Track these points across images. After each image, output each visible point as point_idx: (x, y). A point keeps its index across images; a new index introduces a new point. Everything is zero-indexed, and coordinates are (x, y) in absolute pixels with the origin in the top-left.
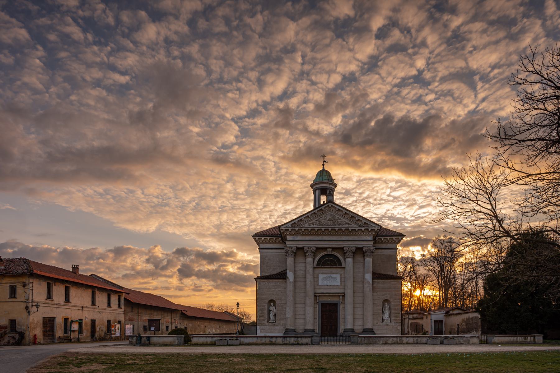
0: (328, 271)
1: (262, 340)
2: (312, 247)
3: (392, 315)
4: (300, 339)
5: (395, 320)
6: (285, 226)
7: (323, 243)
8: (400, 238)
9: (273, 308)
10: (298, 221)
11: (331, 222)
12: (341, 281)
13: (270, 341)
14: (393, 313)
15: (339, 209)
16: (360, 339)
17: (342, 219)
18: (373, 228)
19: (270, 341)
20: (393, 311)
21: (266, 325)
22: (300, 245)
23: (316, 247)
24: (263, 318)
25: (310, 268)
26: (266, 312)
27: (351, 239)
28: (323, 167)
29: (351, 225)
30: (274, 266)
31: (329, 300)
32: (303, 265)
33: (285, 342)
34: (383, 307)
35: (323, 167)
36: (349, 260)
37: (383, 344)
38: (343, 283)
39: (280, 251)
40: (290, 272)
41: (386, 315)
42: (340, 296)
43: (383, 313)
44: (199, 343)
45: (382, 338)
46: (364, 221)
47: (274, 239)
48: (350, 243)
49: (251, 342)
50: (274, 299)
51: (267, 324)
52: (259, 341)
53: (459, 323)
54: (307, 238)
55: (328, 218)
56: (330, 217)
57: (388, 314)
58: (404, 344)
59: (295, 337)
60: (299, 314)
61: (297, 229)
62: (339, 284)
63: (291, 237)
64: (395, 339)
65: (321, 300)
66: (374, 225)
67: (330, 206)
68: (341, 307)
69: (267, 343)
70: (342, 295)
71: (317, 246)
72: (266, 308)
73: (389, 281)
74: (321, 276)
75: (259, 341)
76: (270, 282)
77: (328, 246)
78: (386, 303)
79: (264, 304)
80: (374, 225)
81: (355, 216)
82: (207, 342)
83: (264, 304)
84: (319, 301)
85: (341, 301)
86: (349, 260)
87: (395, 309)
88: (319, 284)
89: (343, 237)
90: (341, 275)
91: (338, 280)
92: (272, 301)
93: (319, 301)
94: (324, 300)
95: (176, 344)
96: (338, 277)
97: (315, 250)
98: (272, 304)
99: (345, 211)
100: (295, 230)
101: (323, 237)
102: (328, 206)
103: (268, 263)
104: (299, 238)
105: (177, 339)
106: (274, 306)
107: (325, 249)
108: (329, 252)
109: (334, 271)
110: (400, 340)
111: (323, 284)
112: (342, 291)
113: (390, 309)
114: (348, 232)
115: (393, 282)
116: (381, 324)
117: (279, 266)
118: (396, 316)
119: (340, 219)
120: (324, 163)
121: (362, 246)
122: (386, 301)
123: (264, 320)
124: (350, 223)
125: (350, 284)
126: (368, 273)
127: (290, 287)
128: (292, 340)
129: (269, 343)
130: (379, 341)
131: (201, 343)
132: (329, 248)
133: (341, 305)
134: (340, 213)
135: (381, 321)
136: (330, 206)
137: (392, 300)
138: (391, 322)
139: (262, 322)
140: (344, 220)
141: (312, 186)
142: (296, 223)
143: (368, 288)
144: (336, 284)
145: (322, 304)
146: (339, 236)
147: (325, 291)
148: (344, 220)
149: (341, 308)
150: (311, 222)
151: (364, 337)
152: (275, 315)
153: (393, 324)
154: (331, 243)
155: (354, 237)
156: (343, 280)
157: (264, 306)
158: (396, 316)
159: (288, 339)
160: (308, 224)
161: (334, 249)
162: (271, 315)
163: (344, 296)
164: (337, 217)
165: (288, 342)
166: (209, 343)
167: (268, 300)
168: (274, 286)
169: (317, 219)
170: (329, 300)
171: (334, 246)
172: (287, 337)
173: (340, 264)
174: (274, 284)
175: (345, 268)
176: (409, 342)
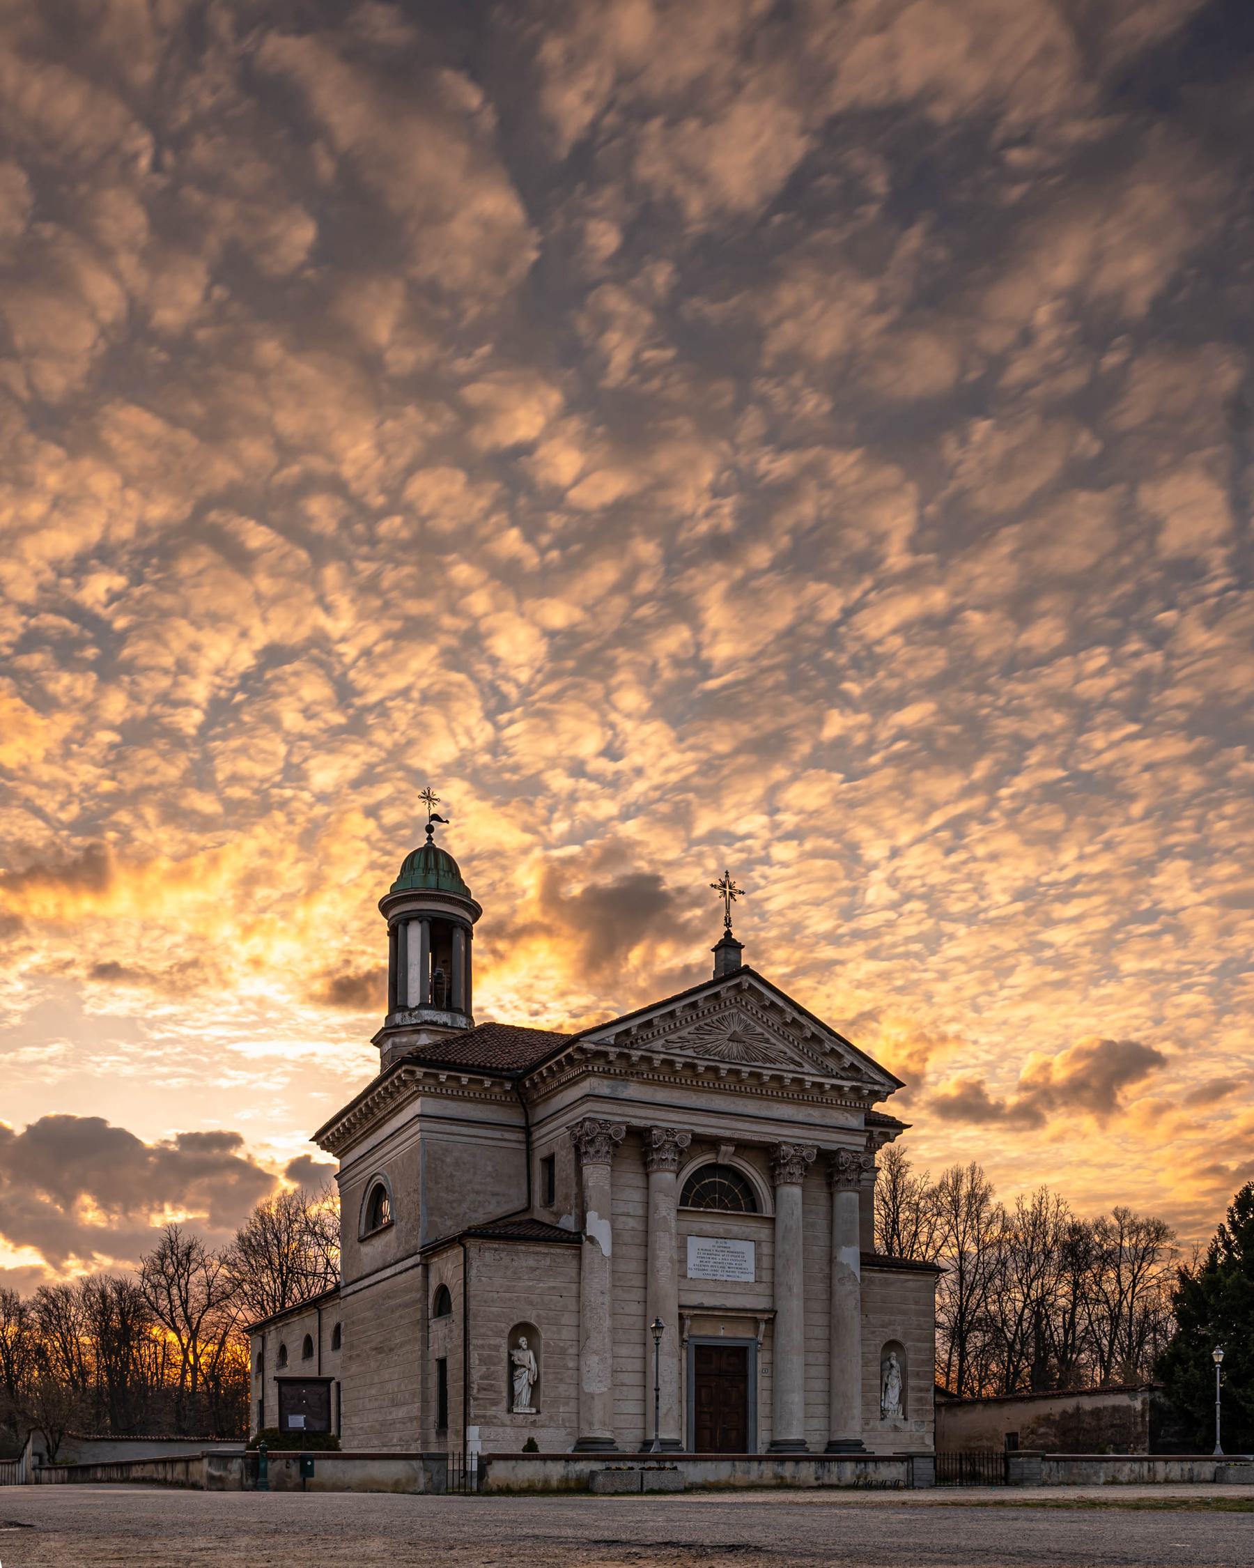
0: (719, 1225)
1: (748, 1473)
2: (681, 1131)
3: (911, 1395)
4: (871, 1466)
5: (917, 1411)
6: (595, 1037)
7: (713, 1121)
8: (891, 1131)
9: (525, 1357)
10: (640, 1026)
11: (741, 1047)
12: (758, 1267)
13: (777, 1476)
14: (913, 1389)
15: (773, 1004)
16: (1045, 1467)
17: (773, 1040)
18: (876, 1088)
19: (777, 1476)
20: (912, 1382)
21: (503, 1425)
22: (640, 1118)
23: (694, 1135)
24: (492, 1396)
25: (666, 1206)
26: (502, 1369)
27: (800, 1118)
28: (430, 839)
29: (800, 1065)
30: (478, 1193)
31: (723, 1333)
32: (637, 1196)
33: (826, 1481)
34: (885, 1367)
35: (430, 839)
36: (792, 1193)
37: (1107, 1483)
38: (766, 1276)
39: (498, 1134)
40: (600, 1217)
41: (893, 1394)
42: (756, 1321)
43: (885, 1387)
44: (515, 1487)
45: (1104, 1465)
46: (849, 1059)
47: (487, 1084)
48: (797, 1132)
49: (712, 1478)
50: (533, 1322)
51: (506, 1418)
52: (739, 1474)
53: (1016, 1429)
54: (662, 1095)
55: (730, 1032)
56: (736, 1028)
57: (897, 1391)
58: (1159, 1483)
59: (858, 1460)
60: (623, 1385)
61: (636, 1054)
62: (751, 1278)
63: (606, 1082)
64: (1136, 1466)
65: (695, 1332)
66: (878, 1077)
67: (745, 986)
68: (761, 1360)
69: (765, 1482)
70: (766, 1316)
71: (699, 1130)
72: (505, 1356)
73: (902, 1277)
74: (694, 1244)
75: (739, 1474)
76: (517, 1253)
77: (727, 1134)
78: (894, 1354)
79: (498, 1341)
80: (878, 1077)
81: (824, 1035)
82: (546, 1481)
83: (498, 1341)
84: (690, 1337)
85: (760, 1338)
86: (792, 1193)
87: (918, 1375)
88: (690, 1274)
89: (775, 1105)
90: (758, 1244)
91: (750, 1264)
92: (524, 1330)
93: (690, 1337)
94: (703, 1333)
95: (422, 1488)
96: (748, 1249)
97: (688, 1143)
98: (523, 1341)
99: (791, 1014)
100: (628, 1057)
101: (715, 1097)
102: (738, 986)
103: (452, 1176)
104: (633, 1090)
105: (426, 1470)
106: (529, 1348)
107: (713, 1143)
108: (726, 1156)
109: (736, 1227)
110: (1149, 1470)
111: (699, 1275)
112: (763, 1303)
113: (904, 1375)
114: (800, 1092)
115: (911, 1282)
116: (878, 1424)
117: (494, 1194)
118: (920, 1400)
119: (767, 1041)
120: (433, 823)
121: (834, 1147)
122: (892, 1345)
123: (495, 1403)
124: (797, 1059)
125: (794, 1278)
126: (848, 1243)
127: (598, 1281)
128: (849, 1471)
129: (774, 1482)
130: (1096, 1473)
131: (525, 1485)
132: (729, 1141)
133: (759, 1355)
134: (773, 1018)
135: (878, 1414)
136: (745, 986)
137: (908, 1344)
138: (905, 1419)
139: (489, 1413)
140: (781, 1046)
141: (385, 906)
142: (634, 1031)
143: (848, 1296)
144: (744, 1278)
145: (699, 1348)
146: (765, 1103)
147: (709, 1301)
148: (781, 1046)
149: (759, 1367)
150: (673, 1037)
151: (1057, 1460)
152: (535, 1386)
153: (910, 1426)
154: (740, 1125)
155: (810, 1111)
156: (766, 1262)
157: (497, 1348)
158: (920, 1400)
159: (834, 1467)
160: (662, 1042)
161: (742, 1146)
162: (522, 1386)
163: (771, 1322)
164: (759, 1030)
165: (834, 1481)
166: (554, 1483)
167: (512, 1324)
168: (534, 1269)
169: (691, 1029)
170: (722, 1333)
171: (748, 1136)
172: (830, 1460)
173: (753, 1205)
174: (531, 1262)
175: (772, 1220)
176: (1172, 1476)
